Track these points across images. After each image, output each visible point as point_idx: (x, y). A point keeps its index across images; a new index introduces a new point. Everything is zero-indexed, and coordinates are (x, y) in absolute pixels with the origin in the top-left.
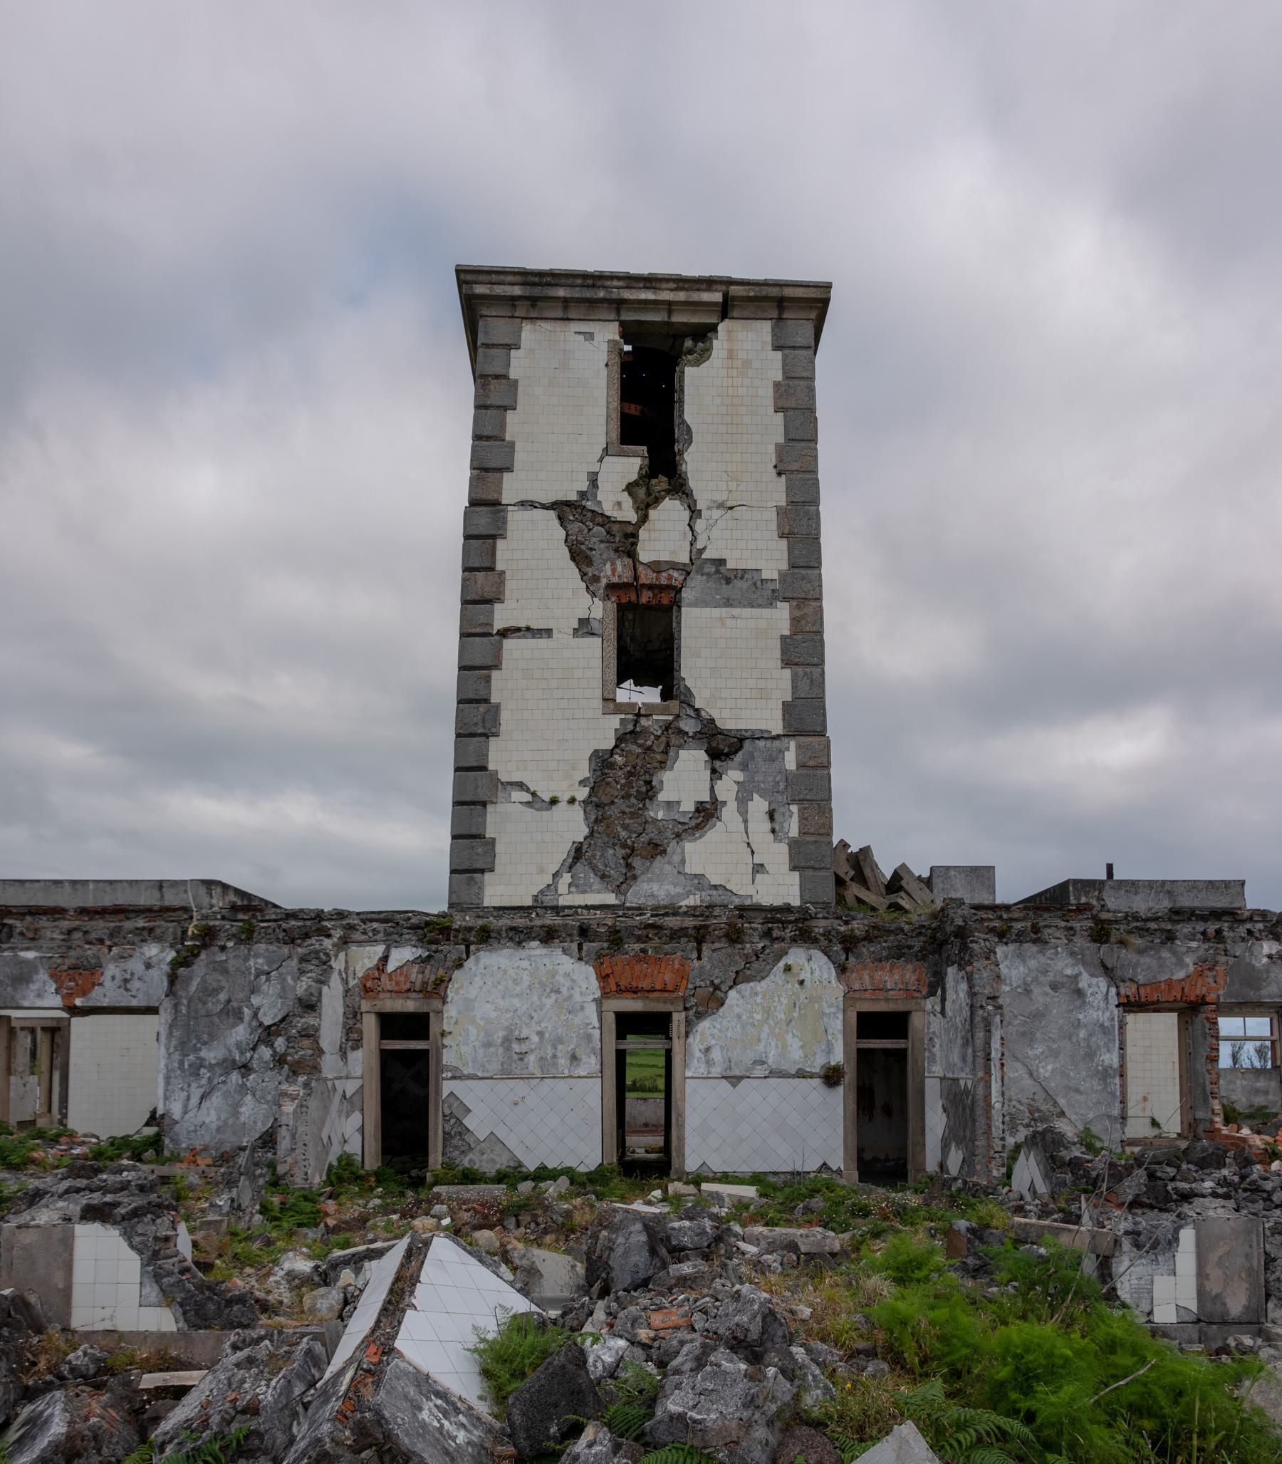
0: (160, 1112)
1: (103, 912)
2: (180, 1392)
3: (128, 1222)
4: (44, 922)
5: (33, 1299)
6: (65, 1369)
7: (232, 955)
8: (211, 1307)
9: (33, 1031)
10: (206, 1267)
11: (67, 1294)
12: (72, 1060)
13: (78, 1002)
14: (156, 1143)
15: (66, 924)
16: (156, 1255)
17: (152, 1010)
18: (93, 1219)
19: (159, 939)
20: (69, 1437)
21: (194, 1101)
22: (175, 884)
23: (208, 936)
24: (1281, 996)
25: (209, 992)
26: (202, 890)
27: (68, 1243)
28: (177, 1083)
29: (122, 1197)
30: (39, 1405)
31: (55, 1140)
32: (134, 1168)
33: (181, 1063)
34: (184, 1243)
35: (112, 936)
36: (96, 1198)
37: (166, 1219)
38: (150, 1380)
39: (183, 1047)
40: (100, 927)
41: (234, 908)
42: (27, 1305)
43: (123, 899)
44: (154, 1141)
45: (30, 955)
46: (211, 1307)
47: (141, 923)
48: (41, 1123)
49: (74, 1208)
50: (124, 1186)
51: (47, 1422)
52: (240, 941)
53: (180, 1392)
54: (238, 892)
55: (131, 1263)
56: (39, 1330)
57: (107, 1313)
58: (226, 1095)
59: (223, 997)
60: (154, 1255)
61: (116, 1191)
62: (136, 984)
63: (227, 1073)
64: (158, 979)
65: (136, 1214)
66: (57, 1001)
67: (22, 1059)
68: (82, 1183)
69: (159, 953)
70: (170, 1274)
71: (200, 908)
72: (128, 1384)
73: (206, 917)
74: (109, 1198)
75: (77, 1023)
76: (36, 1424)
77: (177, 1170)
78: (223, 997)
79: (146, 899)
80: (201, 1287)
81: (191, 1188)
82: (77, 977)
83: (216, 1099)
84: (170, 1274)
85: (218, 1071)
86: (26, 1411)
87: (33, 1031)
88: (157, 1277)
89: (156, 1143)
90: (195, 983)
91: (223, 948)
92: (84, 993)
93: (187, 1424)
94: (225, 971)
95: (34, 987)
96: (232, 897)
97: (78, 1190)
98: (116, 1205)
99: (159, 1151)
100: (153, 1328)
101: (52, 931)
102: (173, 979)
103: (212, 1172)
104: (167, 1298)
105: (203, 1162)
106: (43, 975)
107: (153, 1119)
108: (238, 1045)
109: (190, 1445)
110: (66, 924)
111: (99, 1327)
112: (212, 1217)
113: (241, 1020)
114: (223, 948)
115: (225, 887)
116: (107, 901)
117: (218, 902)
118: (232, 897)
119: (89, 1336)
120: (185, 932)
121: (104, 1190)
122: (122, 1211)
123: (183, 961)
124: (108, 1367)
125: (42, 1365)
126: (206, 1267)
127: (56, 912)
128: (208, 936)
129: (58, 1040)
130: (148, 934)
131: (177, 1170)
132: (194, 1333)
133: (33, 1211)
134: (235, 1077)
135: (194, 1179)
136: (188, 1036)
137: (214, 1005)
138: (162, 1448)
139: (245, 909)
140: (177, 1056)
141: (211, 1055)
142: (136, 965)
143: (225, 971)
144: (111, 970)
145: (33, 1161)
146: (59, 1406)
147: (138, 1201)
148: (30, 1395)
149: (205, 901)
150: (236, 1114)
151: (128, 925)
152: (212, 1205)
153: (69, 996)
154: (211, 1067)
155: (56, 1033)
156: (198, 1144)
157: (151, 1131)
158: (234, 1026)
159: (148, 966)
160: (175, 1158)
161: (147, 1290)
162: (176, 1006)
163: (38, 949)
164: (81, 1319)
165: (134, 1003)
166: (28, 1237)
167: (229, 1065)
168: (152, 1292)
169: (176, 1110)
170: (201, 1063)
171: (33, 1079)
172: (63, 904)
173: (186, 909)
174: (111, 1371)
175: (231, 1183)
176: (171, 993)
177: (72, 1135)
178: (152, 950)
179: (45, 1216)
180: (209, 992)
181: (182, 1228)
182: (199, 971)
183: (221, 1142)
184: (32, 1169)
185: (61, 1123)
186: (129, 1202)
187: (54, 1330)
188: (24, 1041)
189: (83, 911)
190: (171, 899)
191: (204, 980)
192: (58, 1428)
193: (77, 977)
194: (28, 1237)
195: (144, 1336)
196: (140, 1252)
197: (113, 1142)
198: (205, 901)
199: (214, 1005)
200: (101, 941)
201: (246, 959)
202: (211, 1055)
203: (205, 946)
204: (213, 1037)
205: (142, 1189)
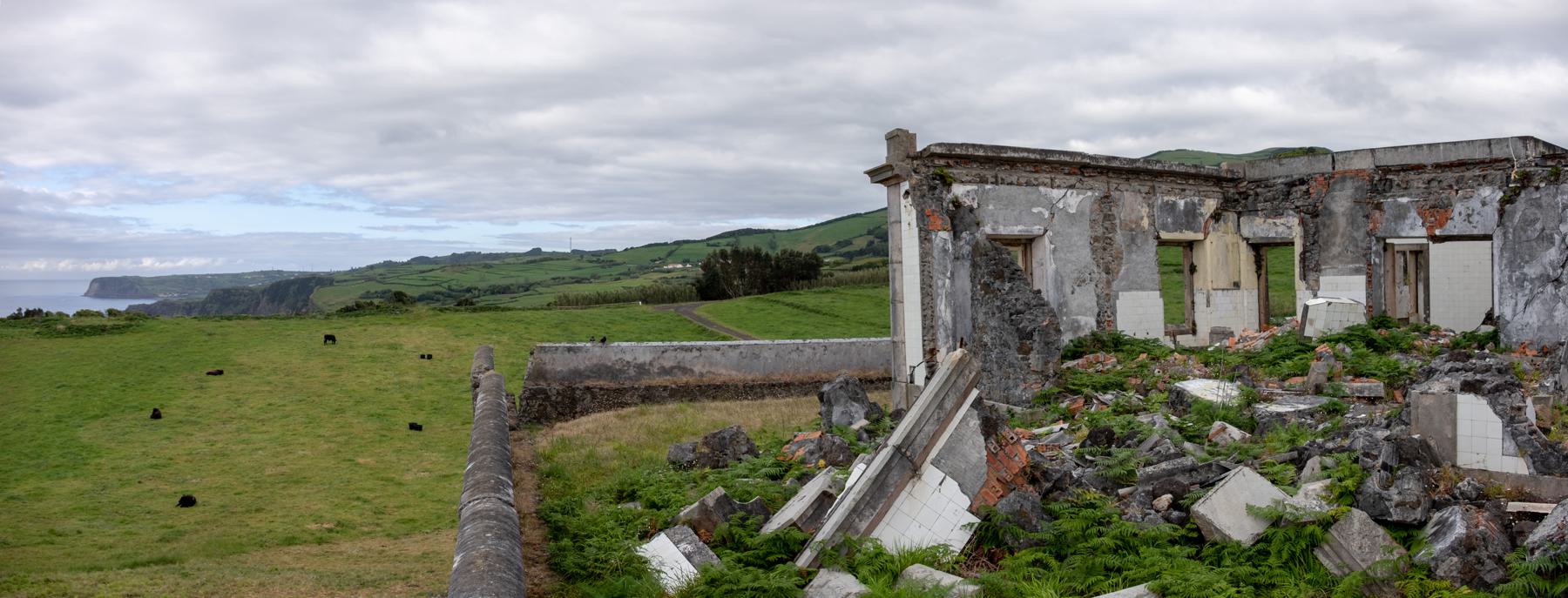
0: (1496, 314)
1: (1451, 166)
2: (1538, 517)
3: (1493, 395)
4: (1412, 175)
5: (1432, 443)
6: (1457, 492)
7: (1544, 193)
8: (1553, 460)
9: (1404, 253)
10: (1546, 431)
11: (1453, 441)
12: (1432, 275)
13: (1437, 232)
14: (1494, 337)
15: (1426, 176)
16: (1512, 419)
17: (1488, 237)
18: (1469, 391)
19: (1491, 183)
20: (1468, 537)
21: (1521, 306)
22: (1499, 141)
23: (1526, 179)
24: (1567, 38)
25: (1528, 222)
26: (1520, 145)
27: (1453, 407)
28: (1508, 292)
29: (1487, 376)
30: (1445, 513)
31: (1427, 333)
32: (1493, 356)
33: (1510, 277)
34: (1531, 412)
35: (1457, 182)
36: (1470, 376)
37: (1518, 394)
38: (1514, 507)
39: (1511, 265)
40: (1450, 176)
41: (1544, 157)
42: (1429, 447)
43: (1464, 155)
44: (1492, 334)
45: (1404, 200)
46: (1553, 460)
47: (1477, 172)
48: (1413, 320)
49: (1457, 383)
50: (1488, 369)
51: (1452, 525)
52: (1550, 182)
53: (1538, 517)
54: (1546, 144)
55: (1496, 424)
56: (1438, 465)
57: (1481, 457)
58: (1544, 302)
59: (1538, 226)
60: (1511, 419)
61: (1483, 372)
62: (1475, 218)
63: (1544, 286)
64: (1491, 212)
65: (1497, 389)
66: (1423, 232)
67: (1399, 274)
68: (1459, 365)
69: (1491, 194)
70: (1523, 434)
71: (1519, 158)
72: (1498, 507)
73: (1524, 165)
74: (1478, 377)
75: (1435, 249)
76: (1444, 527)
77: (1515, 357)
78: (1538, 226)
79: (1480, 154)
80: (1545, 445)
81: (1525, 372)
82: (1436, 212)
83: (1537, 305)
84: (1523, 434)
85: (1537, 283)
86: (1436, 516)
87: (1404, 253)
88: (1514, 436)
89: (1494, 337)
90: (1518, 216)
91: (1537, 188)
92: (1441, 226)
93: (1550, 538)
94: (1540, 206)
95: (1408, 222)
96: (1541, 149)
97: (1457, 370)
98: (1483, 382)
99: (1497, 343)
100: (1512, 471)
101: (1417, 182)
102: (1502, 213)
103: (1539, 361)
104: (1521, 450)
105: (1531, 353)
106: (1413, 214)
107: (1489, 318)
108: (1551, 263)
109: (1552, 552)
110: (1426, 176)
111: (1476, 467)
112: (1541, 395)
113: (1553, 243)
114: (1537, 188)
115: (1536, 141)
116: (1453, 157)
117: (1532, 153)
118: (1541, 149)
119: (1470, 471)
120: (1509, 177)
121: (1475, 370)
122: (1488, 386)
123: (1508, 200)
124: (1483, 495)
125: (1442, 488)
126: (1546, 431)
127: (1419, 168)
128: (1526, 179)
129: (1421, 260)
130: (1484, 180)
131: (1515, 357)
132: (1541, 477)
133: (1429, 383)
134: (1550, 288)
135: (1527, 366)
136: (1516, 255)
137: (1533, 233)
138: (1532, 551)
139: (1553, 157)
140: (1507, 272)
141: (1532, 271)
142: (1475, 204)
143: (1540, 206)
144: (1459, 207)
145: (1415, 347)
146: (1459, 517)
147: (1498, 380)
148: (1437, 506)
149: (1522, 152)
150: (1551, 317)
151: (1468, 174)
152: (1542, 386)
153: (1431, 228)
154: (1532, 281)
155: (1420, 254)
156: (1525, 338)
157: (1490, 328)
158: (1548, 248)
159: (1484, 204)
160: (1508, 350)
161: (1507, 444)
162: (1505, 234)
163: (1409, 195)
164: (1465, 459)
165: (1475, 232)
166: (1427, 401)
167: (1545, 279)
168: (1511, 445)
169: (1508, 313)
170: (1524, 278)
171: (1406, 288)
172: (1423, 162)
173: (1508, 160)
174: (1486, 497)
175: (1554, 370)
176: (1500, 224)
177: (1437, 329)
178: (1486, 192)
179: (1437, 387)
180: (1528, 222)
181: (1529, 401)
182: (1521, 206)
183: (1541, 339)
184: (1415, 353)
185: (1427, 320)
186: (1492, 381)
187: (1447, 464)
188: (1400, 261)
189: (1438, 166)
190: (1498, 153)
191: (1524, 214)
192: (1460, 530)
193: (1436, 212)
194: (1427, 401)
195: (1507, 476)
196: (1502, 417)
197: (1464, 335)
198: (1522, 152)
199: (1533, 233)
200: (1451, 187)
201: (1555, 196)
202: (1532, 271)
203: (1524, 187)
204: (1532, 257)
205: (1500, 371)
